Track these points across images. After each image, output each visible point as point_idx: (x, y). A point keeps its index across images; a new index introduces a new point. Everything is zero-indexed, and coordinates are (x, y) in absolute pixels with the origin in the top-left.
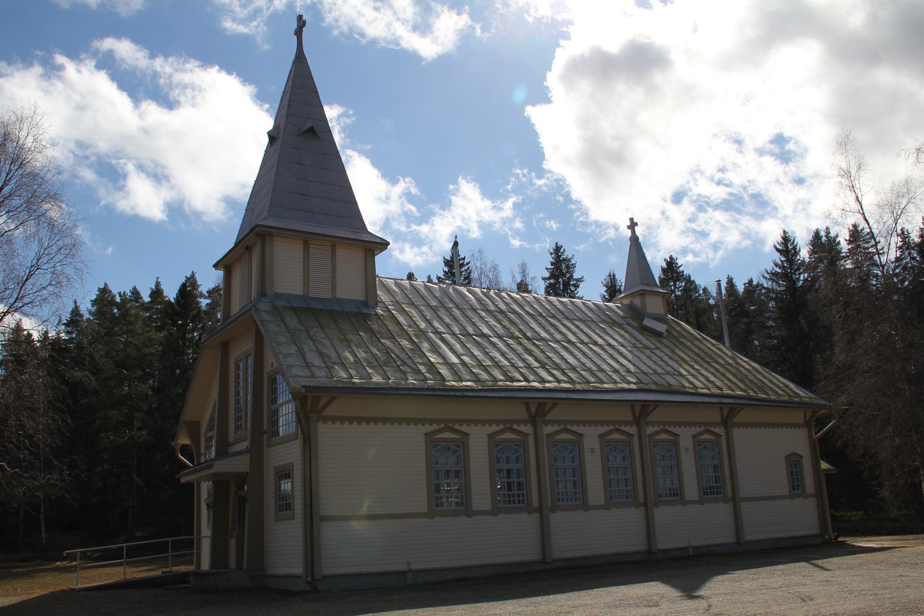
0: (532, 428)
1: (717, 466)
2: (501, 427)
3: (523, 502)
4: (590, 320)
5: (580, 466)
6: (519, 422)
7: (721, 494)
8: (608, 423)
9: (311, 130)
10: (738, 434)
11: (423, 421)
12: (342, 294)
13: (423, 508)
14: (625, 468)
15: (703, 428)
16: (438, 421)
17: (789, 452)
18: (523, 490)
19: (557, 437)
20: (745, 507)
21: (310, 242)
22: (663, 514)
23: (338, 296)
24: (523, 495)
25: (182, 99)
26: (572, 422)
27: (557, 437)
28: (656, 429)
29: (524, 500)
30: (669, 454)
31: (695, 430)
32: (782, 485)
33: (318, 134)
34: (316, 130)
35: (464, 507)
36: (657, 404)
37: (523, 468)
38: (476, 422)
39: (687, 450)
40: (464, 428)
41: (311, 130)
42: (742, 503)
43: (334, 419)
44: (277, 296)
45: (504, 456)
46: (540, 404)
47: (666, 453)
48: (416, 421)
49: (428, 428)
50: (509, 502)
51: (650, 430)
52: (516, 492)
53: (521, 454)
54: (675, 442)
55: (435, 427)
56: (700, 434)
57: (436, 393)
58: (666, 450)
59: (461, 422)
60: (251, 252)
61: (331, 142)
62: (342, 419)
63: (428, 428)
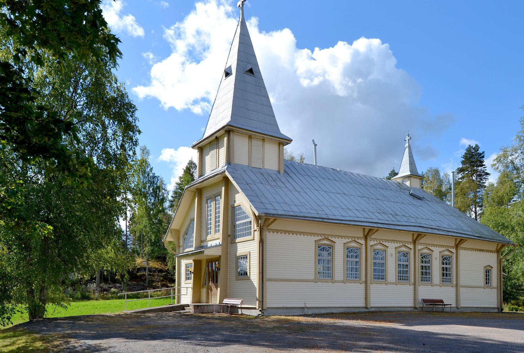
0: (364, 242)
1: (358, 262)
2: (350, 240)
3: (408, 280)
4: (313, 175)
5: (385, 262)
6: (358, 238)
7: (430, 281)
8: (321, 235)
9: (251, 71)
10: (462, 252)
11: (314, 234)
12: (267, 166)
13: (313, 277)
14: (328, 260)
15: (445, 249)
16: (321, 235)
17: (487, 265)
18: (358, 272)
19: (444, 253)
20: (462, 290)
21: (252, 137)
22: (376, 288)
23: (265, 167)
24: (358, 274)
25: (174, 51)
26: (429, 244)
27: (444, 253)
28: (423, 247)
29: (384, 278)
30: (355, 255)
31: (441, 249)
32: (481, 279)
33: (254, 73)
34: (254, 71)
35: (384, 280)
36: (378, 229)
37: (408, 264)
38: (338, 236)
39: (436, 258)
40: (333, 239)
41: (251, 71)
42: (461, 288)
43: (274, 231)
44: (236, 165)
45: (351, 255)
46: (370, 230)
47: (354, 254)
48: (311, 234)
49: (317, 238)
50: (356, 278)
51: (372, 243)
52: (381, 274)
53: (331, 252)
54: (254, 240)
55: (320, 238)
56: (400, 247)
57: (325, 220)
58: (354, 252)
59: (332, 236)
60: (218, 140)
61: (260, 79)
62: (277, 231)
63: (317, 238)
